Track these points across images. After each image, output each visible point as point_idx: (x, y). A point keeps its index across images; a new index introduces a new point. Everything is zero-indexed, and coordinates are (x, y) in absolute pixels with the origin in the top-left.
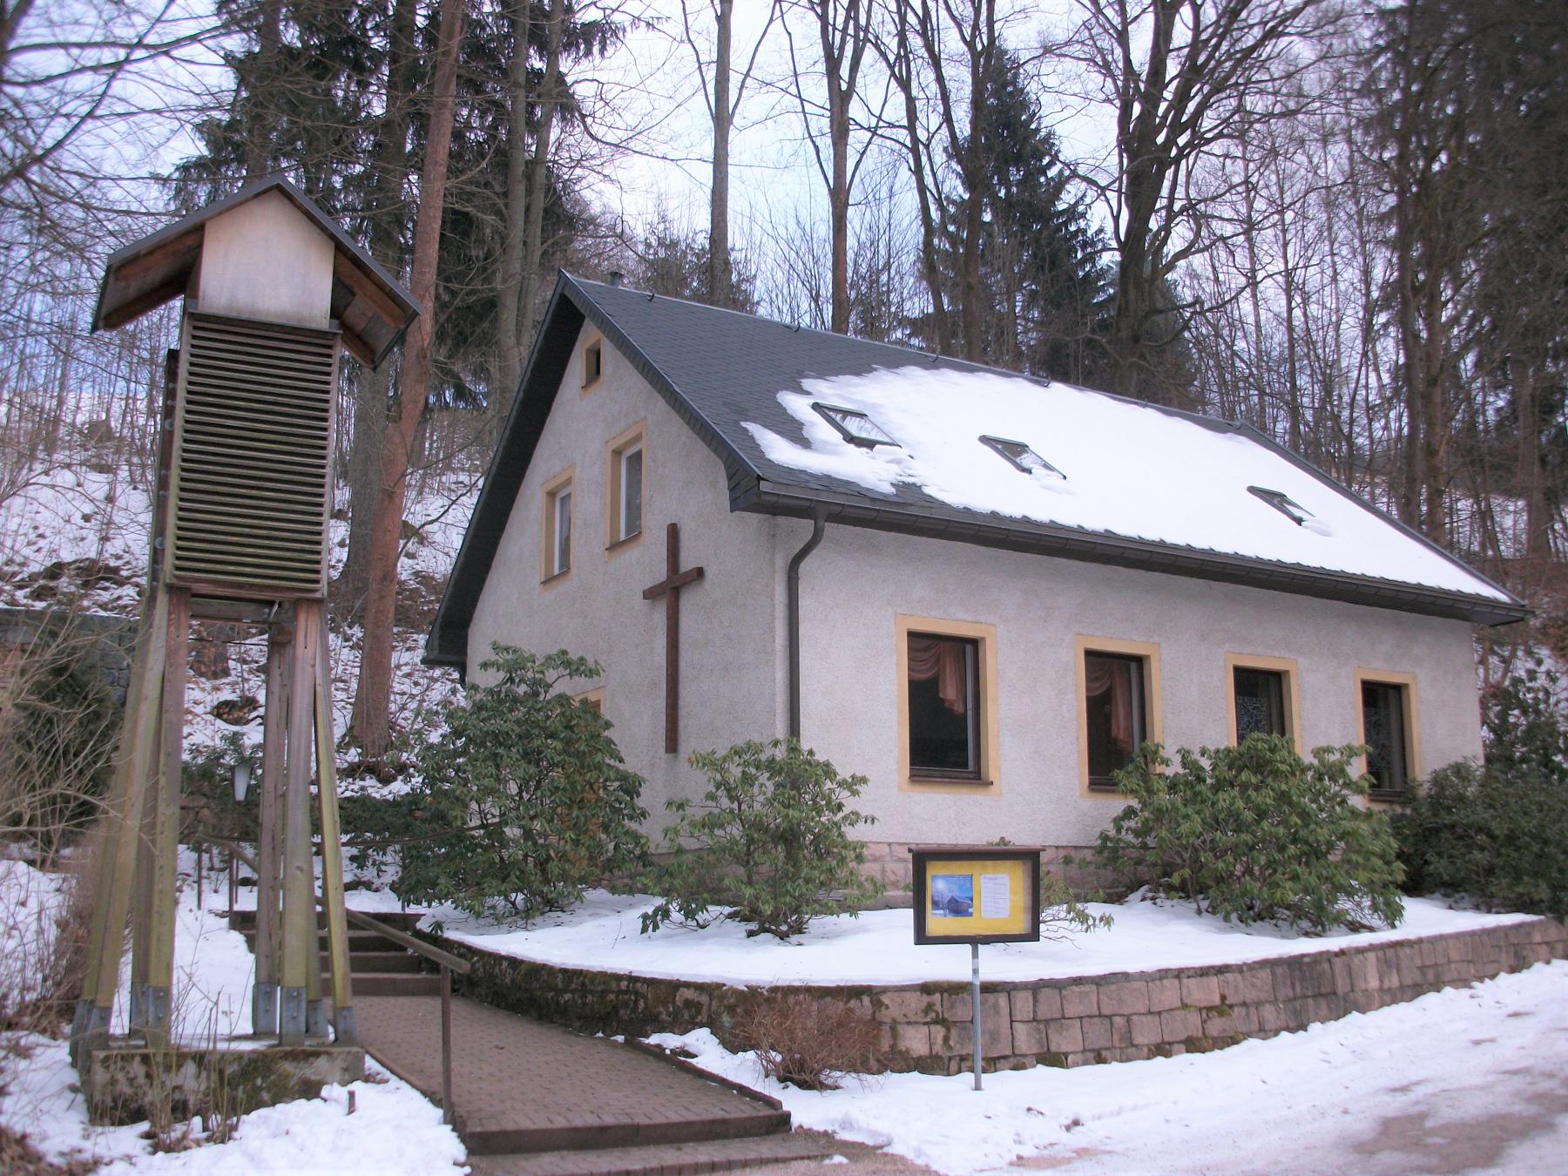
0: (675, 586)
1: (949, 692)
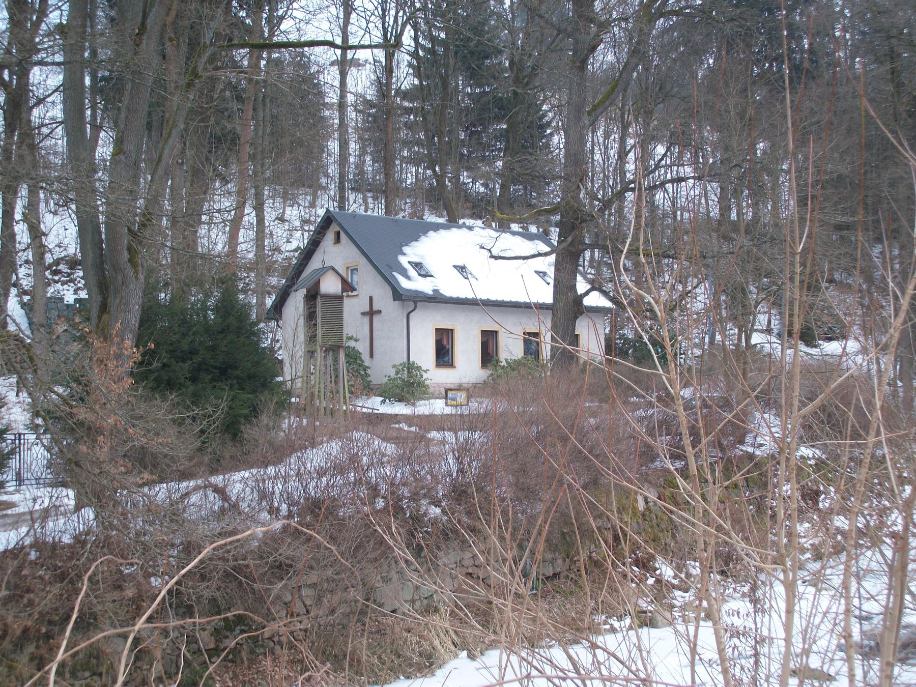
1: (445, 343)
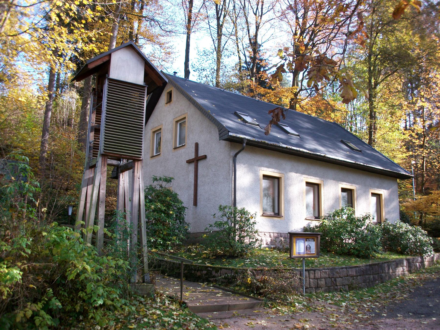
0: (197, 160)
